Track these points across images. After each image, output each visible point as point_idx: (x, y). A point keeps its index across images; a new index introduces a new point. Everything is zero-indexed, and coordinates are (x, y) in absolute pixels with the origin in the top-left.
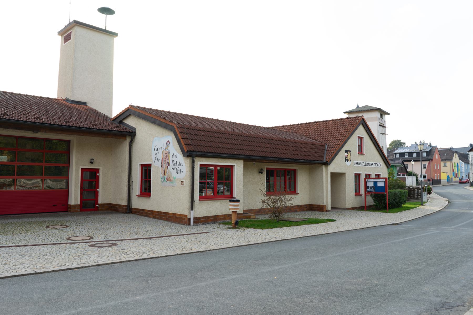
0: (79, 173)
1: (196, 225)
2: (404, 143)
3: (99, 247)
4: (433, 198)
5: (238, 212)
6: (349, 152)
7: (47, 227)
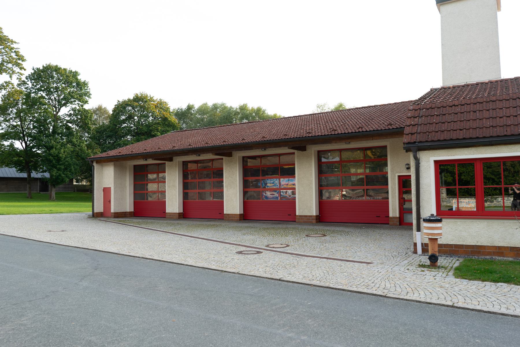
0: (395, 182)
1: (425, 255)
2: (190, 108)
3: (245, 254)
4: (90, 218)
5: (440, 242)
7: (307, 236)
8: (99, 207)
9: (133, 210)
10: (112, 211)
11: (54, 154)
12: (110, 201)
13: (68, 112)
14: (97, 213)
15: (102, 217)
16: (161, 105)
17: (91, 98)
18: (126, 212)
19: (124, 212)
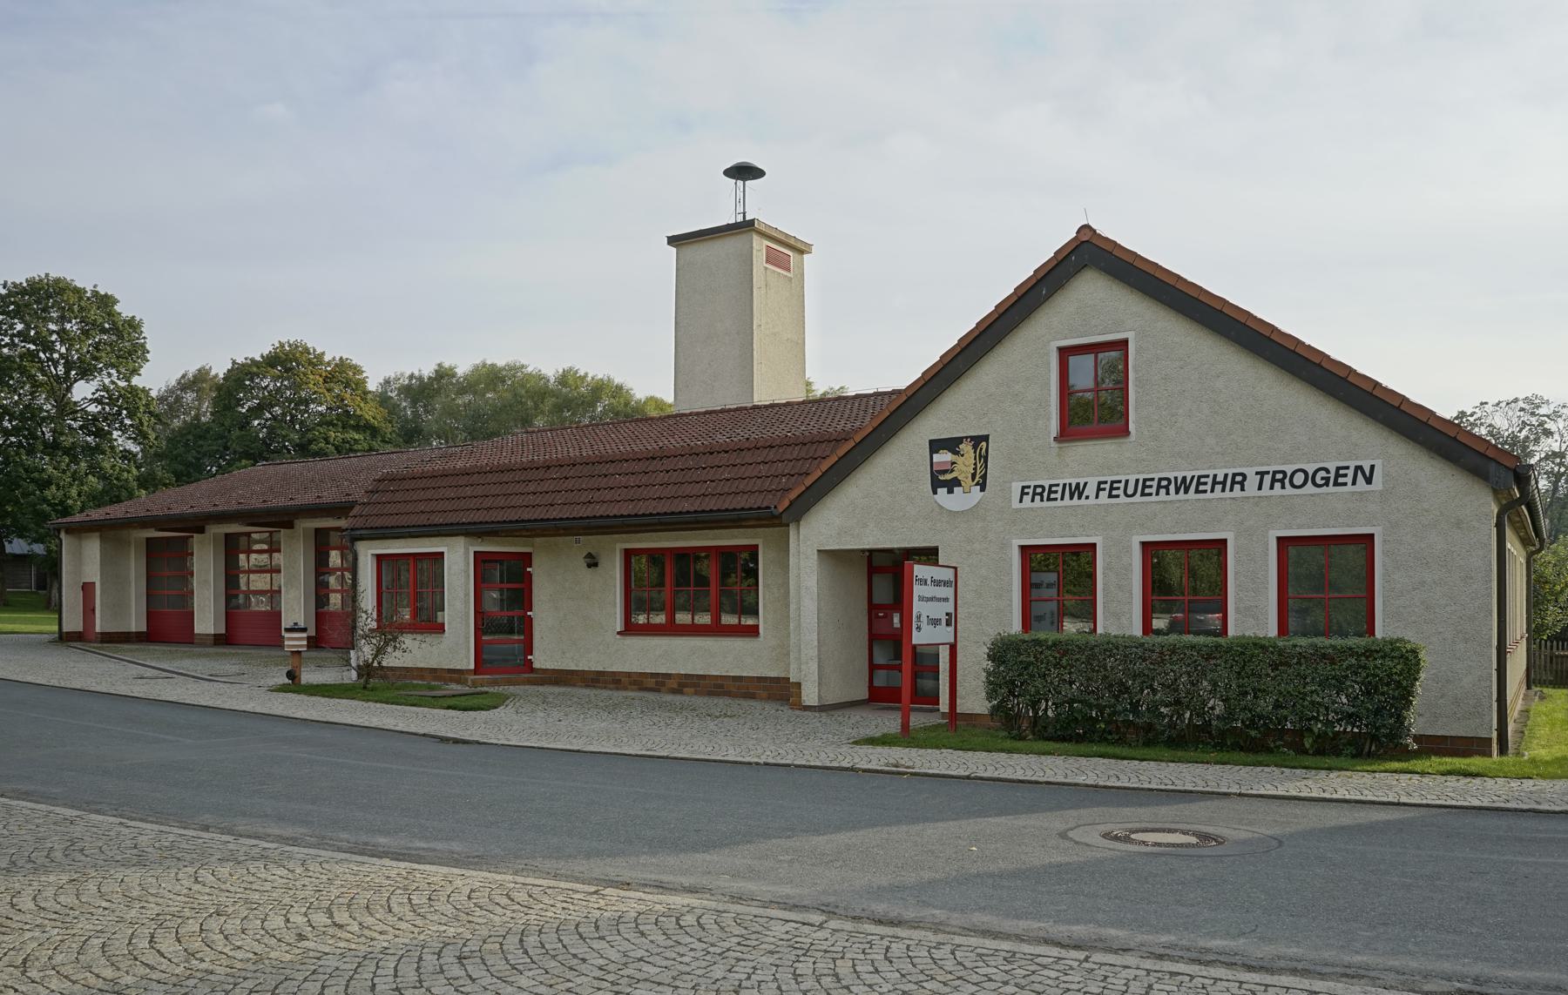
6: (966, 448)
8: (73, 623)
9: (144, 629)
10: (98, 629)
11: (54, 498)
12: (94, 610)
13: (93, 394)
14: (67, 633)
15: (80, 641)
16: (344, 375)
17: (148, 361)
18: (129, 633)
19: (124, 633)
